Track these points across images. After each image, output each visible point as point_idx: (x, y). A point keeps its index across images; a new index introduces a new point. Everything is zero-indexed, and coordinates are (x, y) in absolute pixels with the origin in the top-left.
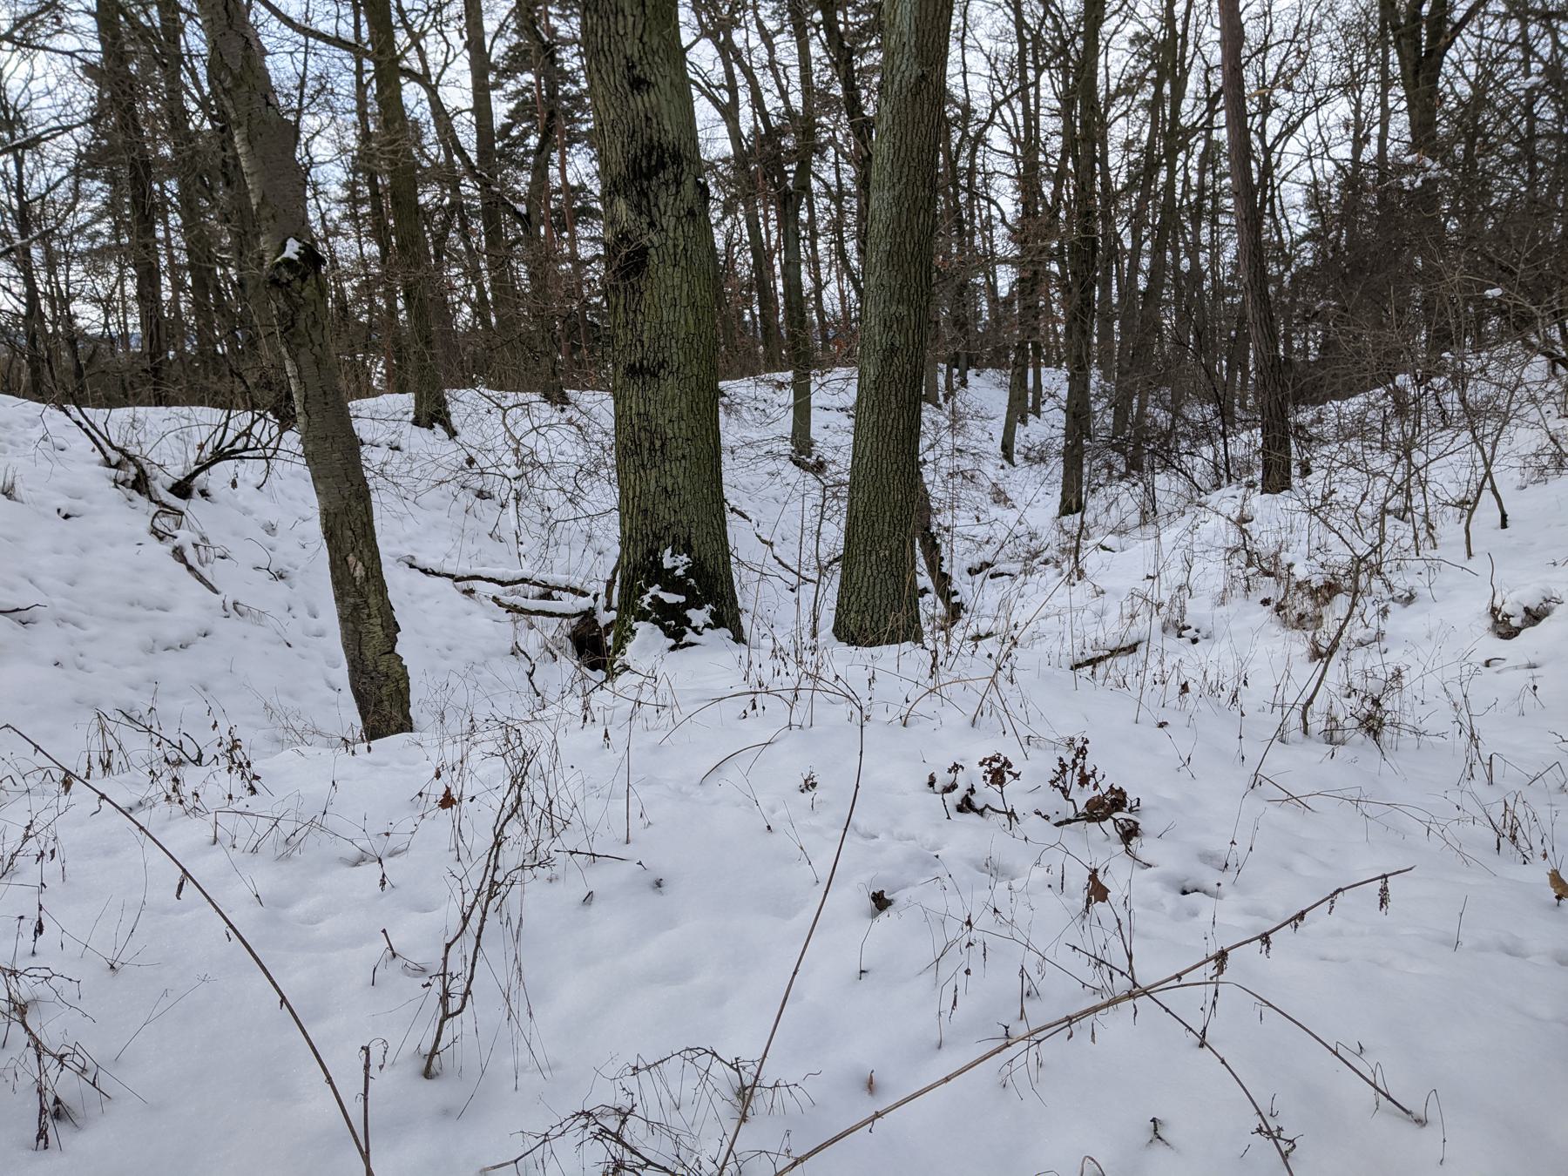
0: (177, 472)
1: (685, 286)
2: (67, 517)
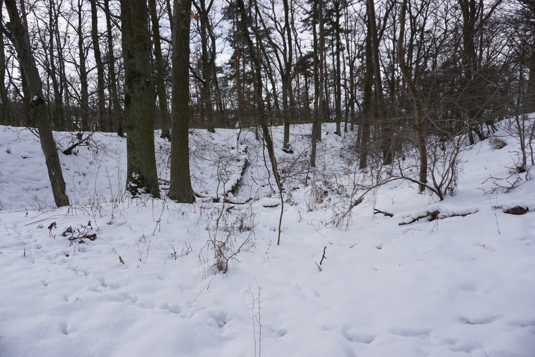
0: (66, 148)
1: (140, 106)
2: (25, 158)
